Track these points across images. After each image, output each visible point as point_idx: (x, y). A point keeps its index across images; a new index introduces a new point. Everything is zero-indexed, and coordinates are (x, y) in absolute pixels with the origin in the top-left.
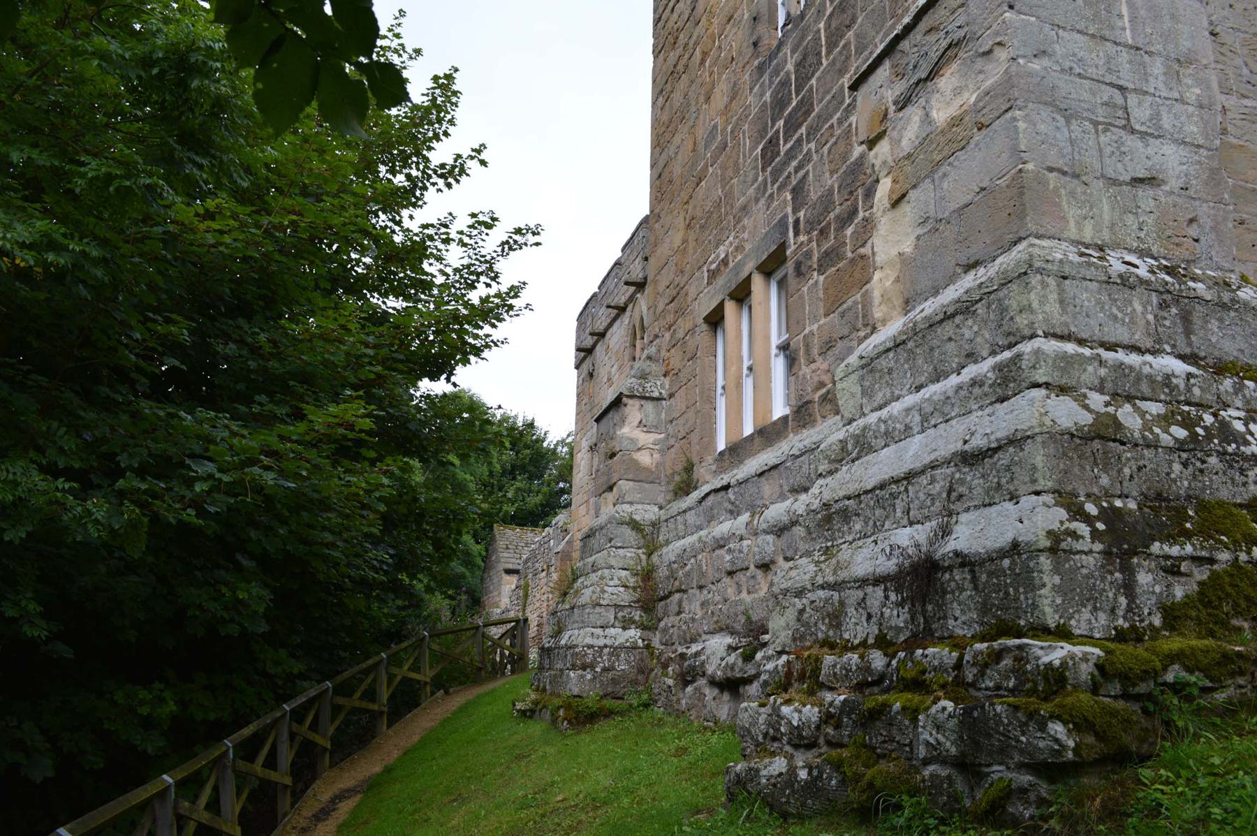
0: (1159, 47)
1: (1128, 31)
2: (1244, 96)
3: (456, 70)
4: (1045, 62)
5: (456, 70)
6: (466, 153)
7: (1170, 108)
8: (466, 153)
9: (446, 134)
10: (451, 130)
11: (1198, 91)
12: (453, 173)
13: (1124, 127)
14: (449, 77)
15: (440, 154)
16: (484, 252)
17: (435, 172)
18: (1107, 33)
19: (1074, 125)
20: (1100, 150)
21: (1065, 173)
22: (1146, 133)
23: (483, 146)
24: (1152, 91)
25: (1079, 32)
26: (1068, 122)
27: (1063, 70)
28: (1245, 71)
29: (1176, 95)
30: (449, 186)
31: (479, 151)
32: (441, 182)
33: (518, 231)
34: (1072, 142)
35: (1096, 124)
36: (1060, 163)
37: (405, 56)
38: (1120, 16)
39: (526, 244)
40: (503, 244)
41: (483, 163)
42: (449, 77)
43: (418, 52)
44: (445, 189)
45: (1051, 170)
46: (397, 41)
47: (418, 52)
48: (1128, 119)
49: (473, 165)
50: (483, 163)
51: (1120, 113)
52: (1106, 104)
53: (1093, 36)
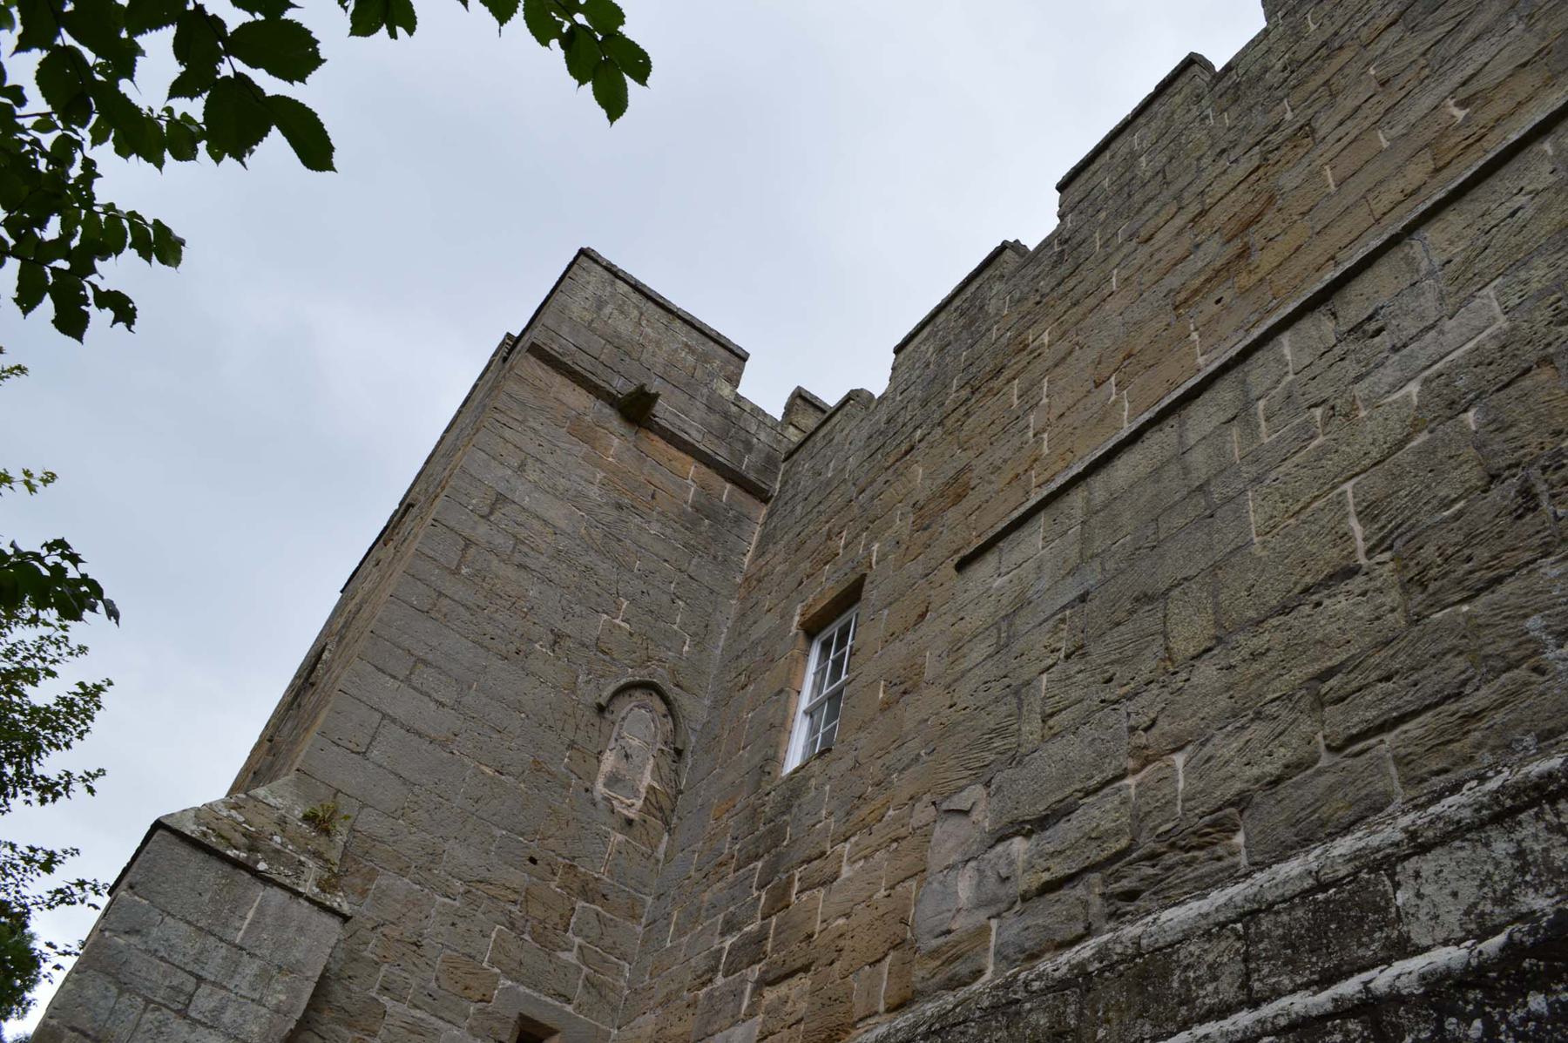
0: (266, 952)
1: (241, 933)
2: (416, 1007)
3: (110, 684)
4: (134, 940)
5: (110, 684)
6: (77, 773)
7: (241, 1005)
8: (77, 773)
9: (67, 745)
10: (75, 743)
11: (283, 997)
12: (49, 791)
13: (178, 1012)
14: (99, 688)
15: (50, 765)
16: (24, 892)
17: (35, 781)
18: (217, 929)
19: (125, 999)
20: (138, 1025)
21: (86, 1035)
22: (199, 1022)
23: (101, 772)
24: (231, 987)
25: (189, 923)
26: (120, 994)
27: (147, 951)
28: (433, 984)
29: (257, 996)
30: (43, 801)
31: (94, 777)
32: (36, 795)
33: (81, 884)
34: (112, 1011)
35: (148, 1001)
36: (87, 1026)
37: (65, 650)
38: (243, 918)
39: (82, 901)
40: (59, 891)
41: (91, 790)
42: (99, 688)
43: (83, 649)
44: (36, 804)
45: (73, 1029)
46: (61, 632)
47: (83, 649)
48: (187, 1006)
49: (78, 788)
50: (91, 790)
51: (182, 998)
52: (172, 988)
53: (201, 929)
